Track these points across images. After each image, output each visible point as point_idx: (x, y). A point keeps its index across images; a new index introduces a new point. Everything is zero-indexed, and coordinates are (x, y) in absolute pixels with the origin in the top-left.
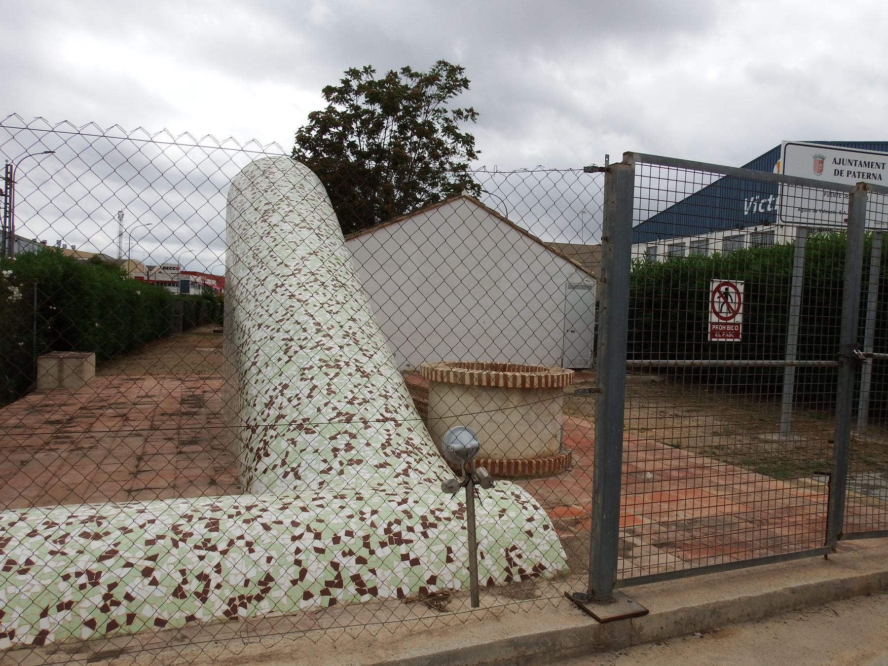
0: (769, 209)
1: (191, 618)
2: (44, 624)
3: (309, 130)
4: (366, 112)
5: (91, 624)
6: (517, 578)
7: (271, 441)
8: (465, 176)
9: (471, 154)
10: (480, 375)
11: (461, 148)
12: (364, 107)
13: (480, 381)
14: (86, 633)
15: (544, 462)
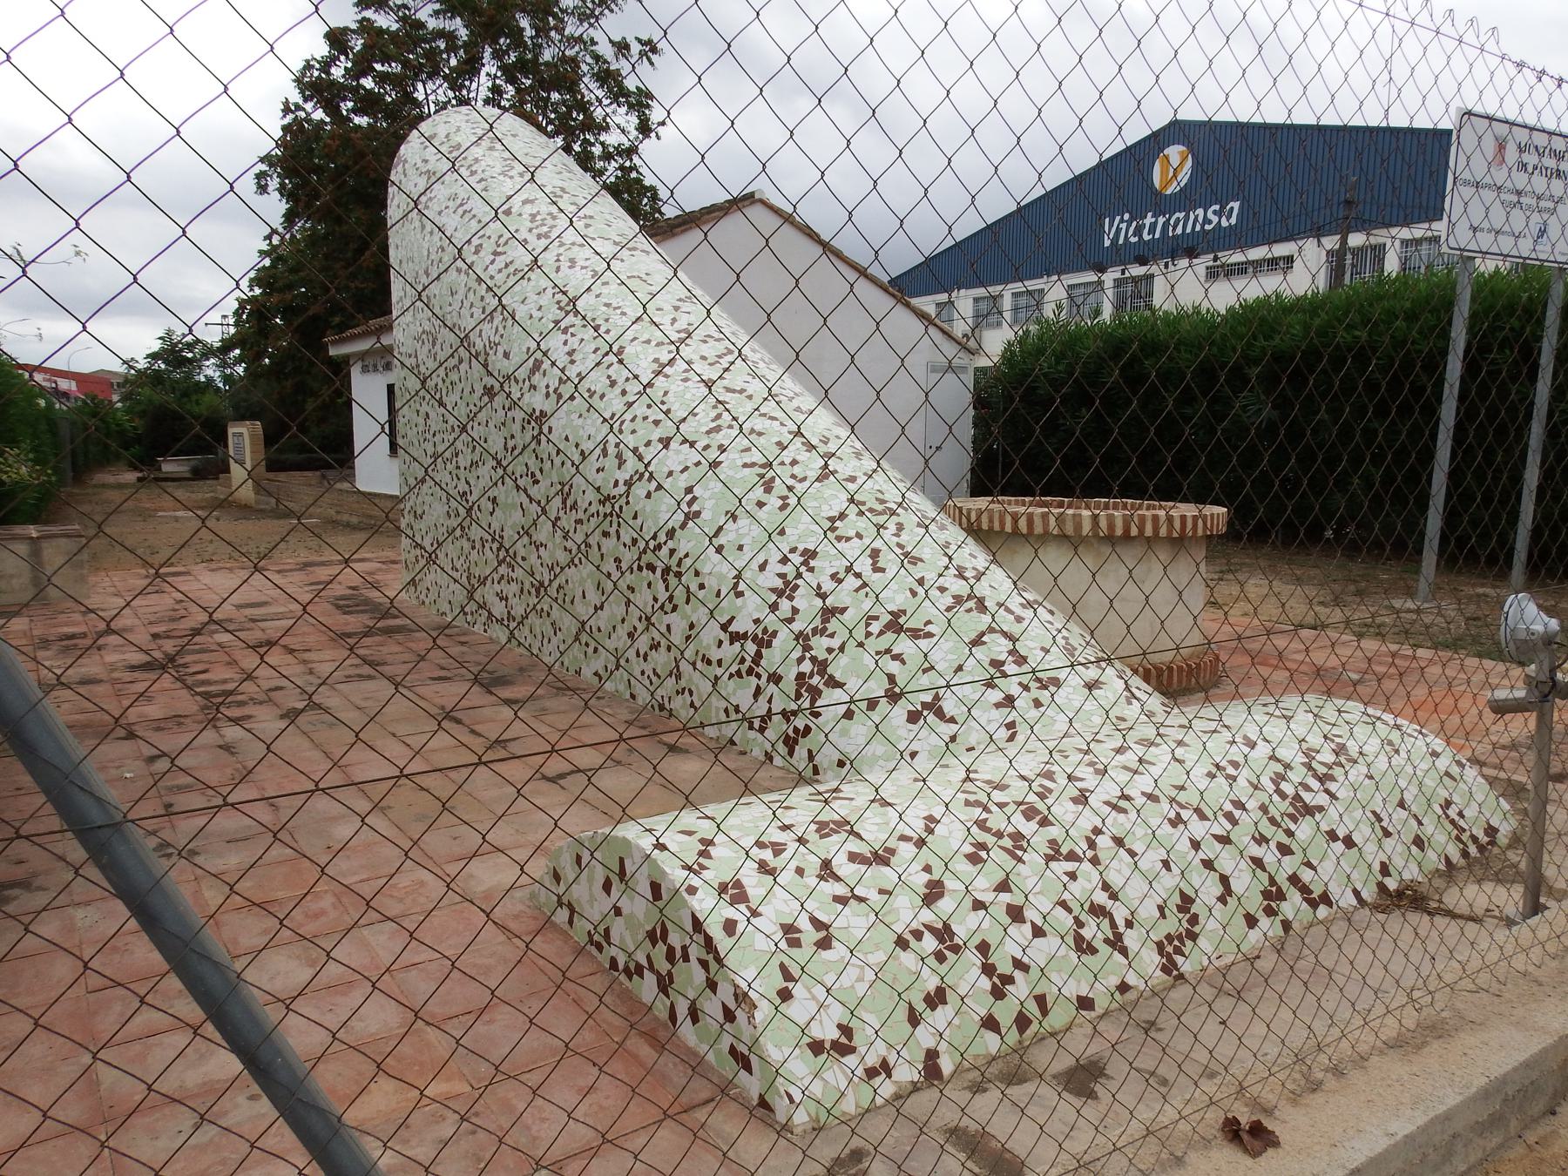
0: (1146, 237)
1: (1123, 987)
2: (925, 1037)
3: (327, 64)
4: (441, 34)
5: (990, 1023)
6: (1473, 850)
7: (830, 658)
8: (631, 169)
9: (645, 129)
10: (1045, 516)
11: (623, 118)
12: (432, 24)
13: (1111, 526)
14: (992, 1042)
15: (1198, 665)
